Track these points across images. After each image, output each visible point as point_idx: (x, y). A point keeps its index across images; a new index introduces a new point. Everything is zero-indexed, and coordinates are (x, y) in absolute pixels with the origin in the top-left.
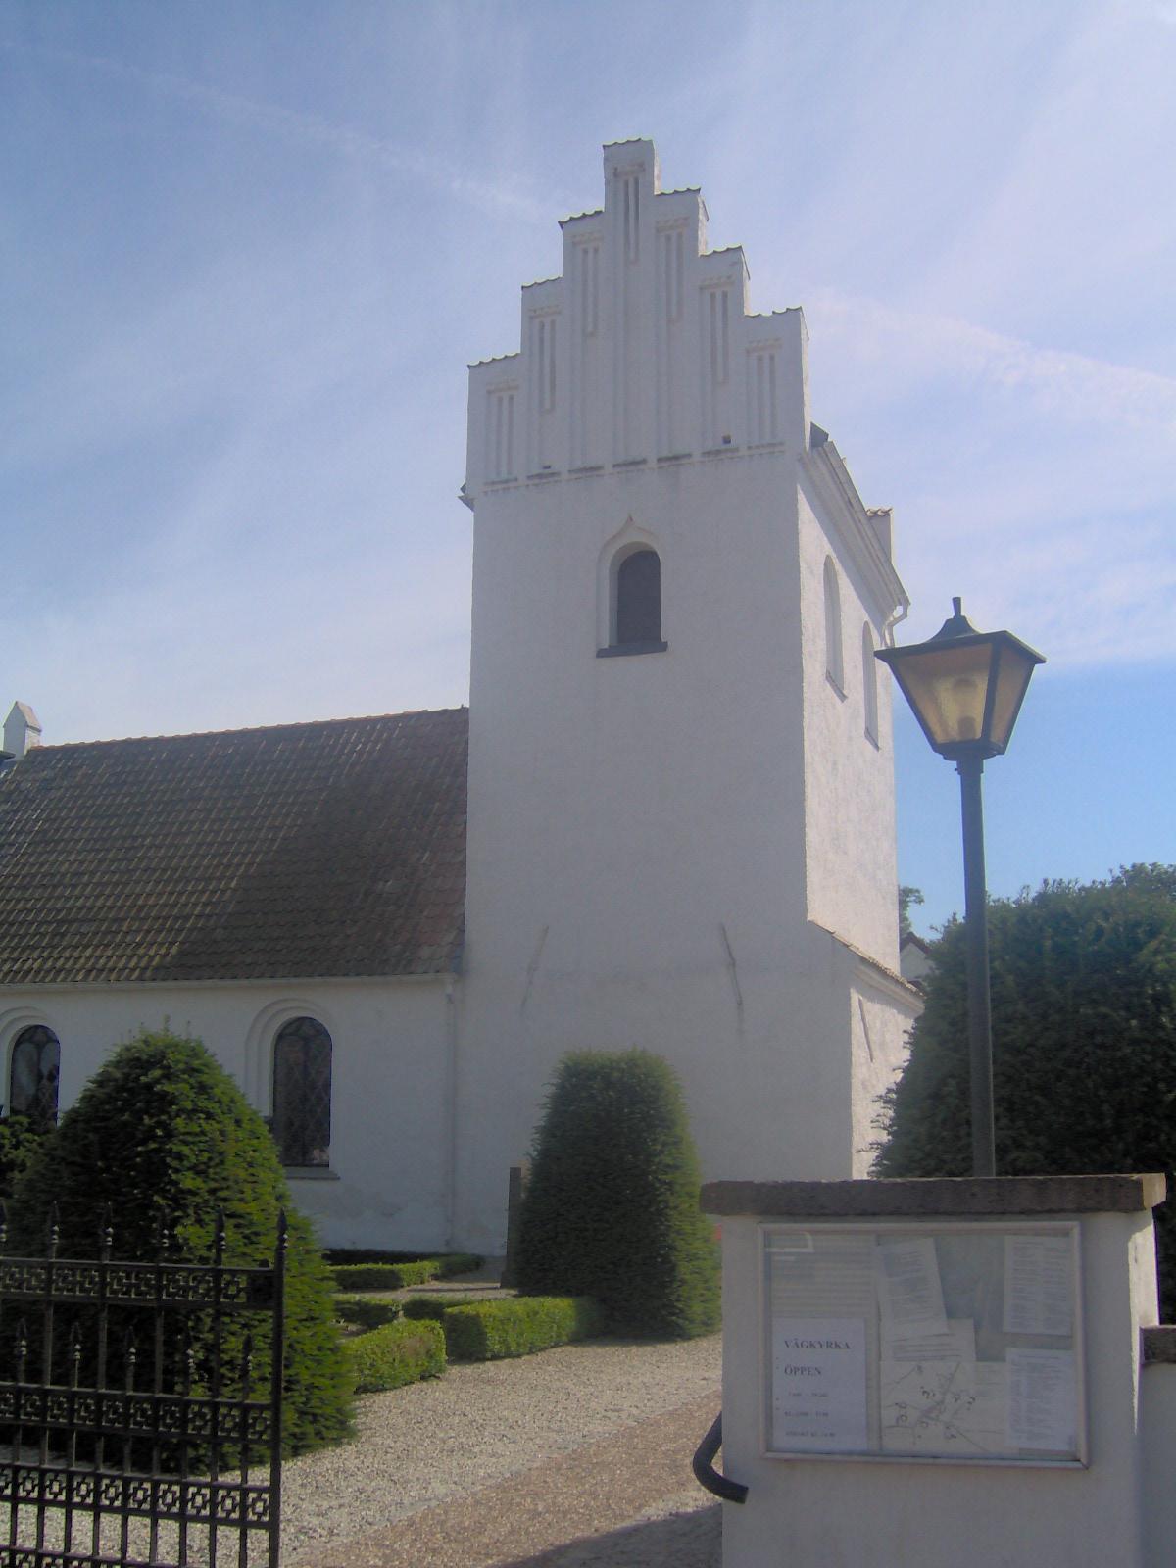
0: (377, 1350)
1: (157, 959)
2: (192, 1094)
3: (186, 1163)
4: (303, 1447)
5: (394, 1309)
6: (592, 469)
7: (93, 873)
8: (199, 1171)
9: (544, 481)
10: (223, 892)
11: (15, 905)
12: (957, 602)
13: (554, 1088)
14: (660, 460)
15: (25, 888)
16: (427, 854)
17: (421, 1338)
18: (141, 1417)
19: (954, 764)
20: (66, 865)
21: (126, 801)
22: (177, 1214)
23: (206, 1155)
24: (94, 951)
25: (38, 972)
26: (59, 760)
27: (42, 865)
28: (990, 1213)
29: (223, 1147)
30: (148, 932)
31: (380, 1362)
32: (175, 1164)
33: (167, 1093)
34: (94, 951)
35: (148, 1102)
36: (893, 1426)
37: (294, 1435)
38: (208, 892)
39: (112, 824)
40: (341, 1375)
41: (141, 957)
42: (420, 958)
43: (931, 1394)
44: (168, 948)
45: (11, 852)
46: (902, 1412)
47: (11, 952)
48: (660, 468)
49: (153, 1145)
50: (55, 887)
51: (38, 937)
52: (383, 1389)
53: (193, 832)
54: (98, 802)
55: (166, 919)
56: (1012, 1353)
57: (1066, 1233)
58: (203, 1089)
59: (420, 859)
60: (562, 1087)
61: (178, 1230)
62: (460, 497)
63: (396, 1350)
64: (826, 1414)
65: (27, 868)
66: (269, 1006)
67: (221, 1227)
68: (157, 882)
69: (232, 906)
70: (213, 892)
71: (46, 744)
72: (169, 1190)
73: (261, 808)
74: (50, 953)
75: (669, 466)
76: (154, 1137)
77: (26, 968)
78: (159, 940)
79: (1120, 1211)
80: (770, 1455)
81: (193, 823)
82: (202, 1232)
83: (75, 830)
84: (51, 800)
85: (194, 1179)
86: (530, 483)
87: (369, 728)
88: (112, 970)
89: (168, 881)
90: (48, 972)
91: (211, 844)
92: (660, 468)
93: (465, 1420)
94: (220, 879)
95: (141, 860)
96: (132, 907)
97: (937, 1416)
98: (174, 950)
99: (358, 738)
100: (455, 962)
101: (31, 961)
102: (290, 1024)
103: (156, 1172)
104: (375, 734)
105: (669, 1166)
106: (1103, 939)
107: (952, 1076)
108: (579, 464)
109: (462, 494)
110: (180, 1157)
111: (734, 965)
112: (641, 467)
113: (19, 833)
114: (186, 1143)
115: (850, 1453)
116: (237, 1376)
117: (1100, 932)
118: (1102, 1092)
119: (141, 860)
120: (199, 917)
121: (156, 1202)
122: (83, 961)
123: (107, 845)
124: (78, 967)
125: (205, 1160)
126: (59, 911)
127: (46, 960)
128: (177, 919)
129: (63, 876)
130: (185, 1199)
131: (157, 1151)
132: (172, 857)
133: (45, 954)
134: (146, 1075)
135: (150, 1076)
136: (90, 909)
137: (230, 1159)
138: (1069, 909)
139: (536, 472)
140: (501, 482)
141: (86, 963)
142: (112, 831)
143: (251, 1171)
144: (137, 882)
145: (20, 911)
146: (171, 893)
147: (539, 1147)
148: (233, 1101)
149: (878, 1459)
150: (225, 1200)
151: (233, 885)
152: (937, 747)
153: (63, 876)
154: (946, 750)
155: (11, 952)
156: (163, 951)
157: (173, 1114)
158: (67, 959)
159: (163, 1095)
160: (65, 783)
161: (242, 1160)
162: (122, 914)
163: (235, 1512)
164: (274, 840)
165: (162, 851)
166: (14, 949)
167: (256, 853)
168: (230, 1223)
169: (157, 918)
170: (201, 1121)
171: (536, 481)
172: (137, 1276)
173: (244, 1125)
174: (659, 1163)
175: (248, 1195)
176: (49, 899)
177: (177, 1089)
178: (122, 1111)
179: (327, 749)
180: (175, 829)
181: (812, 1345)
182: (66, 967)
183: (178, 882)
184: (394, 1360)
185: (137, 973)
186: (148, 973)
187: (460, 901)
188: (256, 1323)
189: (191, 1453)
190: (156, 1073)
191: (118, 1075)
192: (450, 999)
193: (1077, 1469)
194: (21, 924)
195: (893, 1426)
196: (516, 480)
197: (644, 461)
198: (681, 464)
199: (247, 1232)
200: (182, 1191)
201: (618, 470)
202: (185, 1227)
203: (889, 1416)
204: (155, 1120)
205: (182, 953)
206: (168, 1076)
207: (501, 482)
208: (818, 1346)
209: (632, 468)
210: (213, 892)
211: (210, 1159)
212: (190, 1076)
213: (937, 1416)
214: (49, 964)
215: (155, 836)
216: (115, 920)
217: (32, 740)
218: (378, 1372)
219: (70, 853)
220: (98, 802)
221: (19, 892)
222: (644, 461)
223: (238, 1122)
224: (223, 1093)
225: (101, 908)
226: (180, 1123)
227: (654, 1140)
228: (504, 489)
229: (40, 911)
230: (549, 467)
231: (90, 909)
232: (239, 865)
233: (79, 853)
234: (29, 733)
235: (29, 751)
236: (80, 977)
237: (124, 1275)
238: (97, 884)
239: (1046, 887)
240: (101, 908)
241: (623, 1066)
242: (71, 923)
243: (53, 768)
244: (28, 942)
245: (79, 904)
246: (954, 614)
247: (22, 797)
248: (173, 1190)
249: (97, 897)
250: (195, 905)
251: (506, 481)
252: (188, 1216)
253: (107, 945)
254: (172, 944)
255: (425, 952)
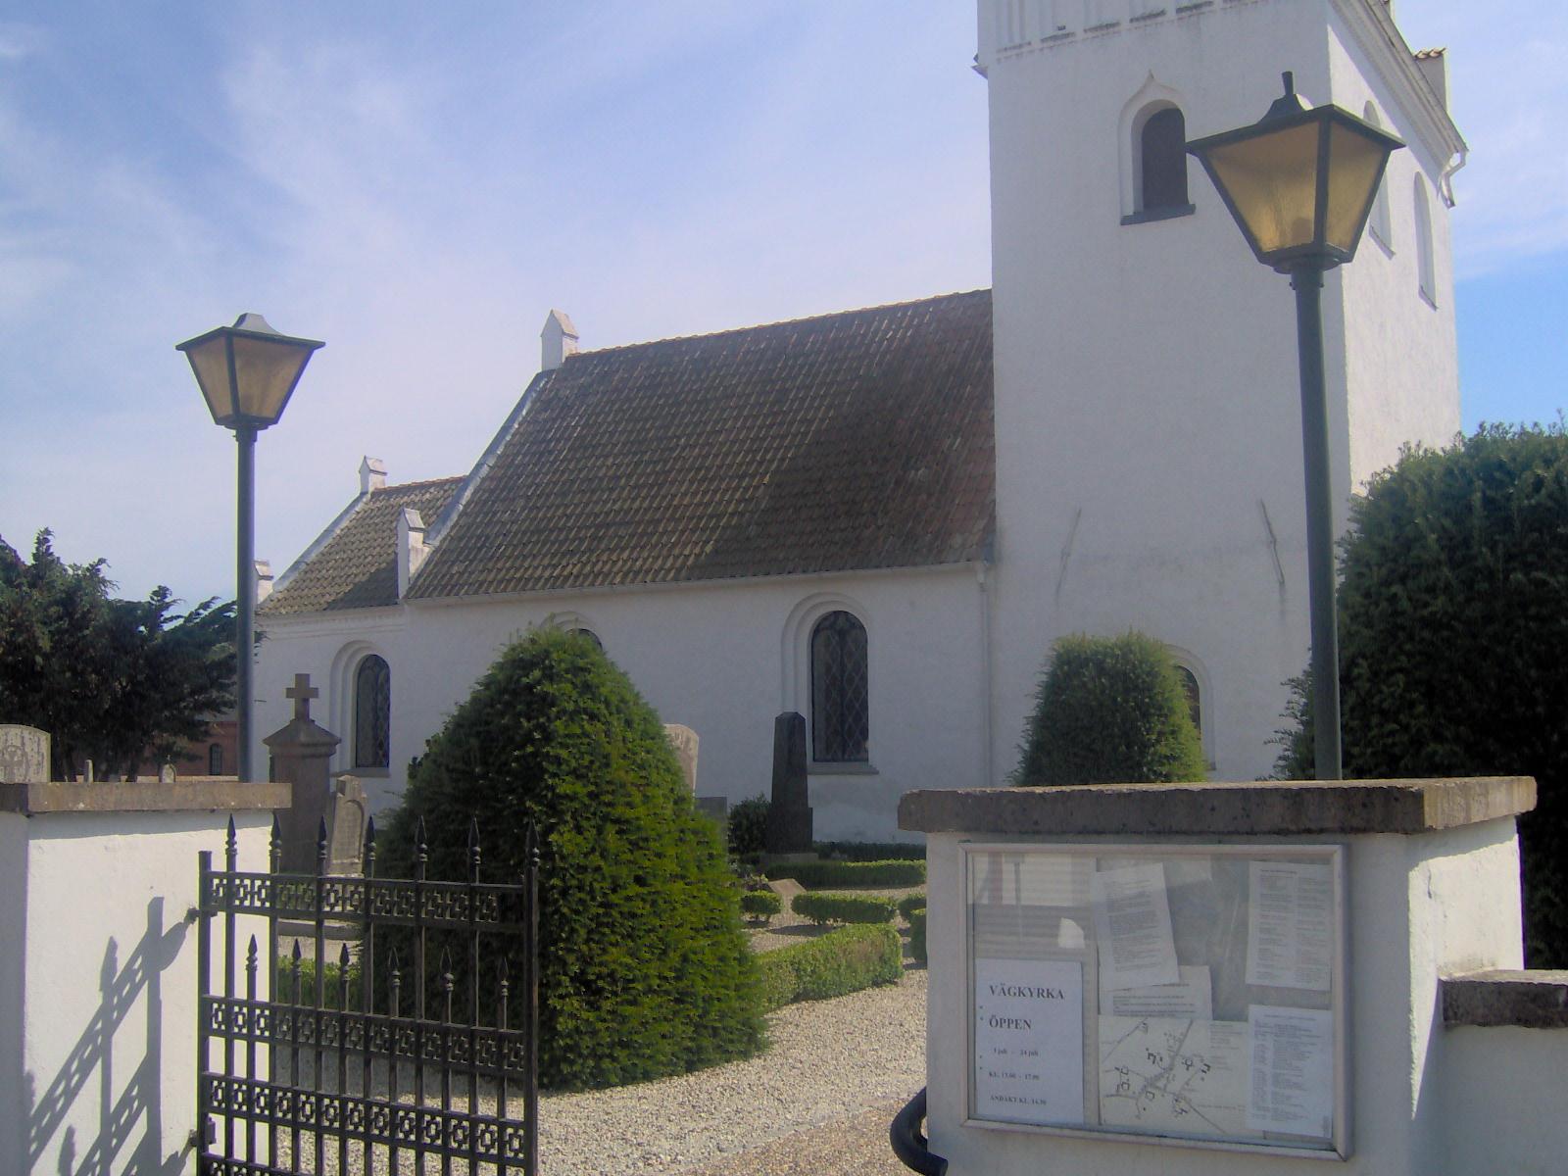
0: (819, 956)
1: (692, 559)
2: (575, 695)
3: (564, 767)
4: (701, 1061)
5: (890, 908)
6: (1108, 26)
7: (630, 476)
8: (577, 774)
9: (1059, 42)
10: (757, 488)
11: (555, 512)
12: (1288, 78)
13: (1045, 676)
14: (1179, 10)
15: (564, 494)
16: (959, 440)
17: (873, 942)
18: (406, 1044)
19: (1287, 278)
20: (604, 470)
21: (661, 402)
22: (552, 821)
23: (587, 758)
24: (631, 552)
25: (577, 577)
26: (596, 366)
27: (580, 471)
28: (1237, 832)
29: (608, 748)
30: (683, 532)
31: (822, 968)
32: (552, 768)
33: (547, 693)
34: (631, 552)
35: (529, 704)
36: (1112, 1095)
37: (688, 1049)
38: (710, 492)
39: (648, 426)
40: (749, 986)
41: (676, 558)
42: (950, 547)
43: (1158, 1058)
44: (702, 548)
45: (551, 459)
46: (1124, 1078)
47: (552, 559)
48: (1180, 19)
49: (530, 749)
50: (593, 492)
51: (577, 542)
52: (827, 997)
53: (726, 430)
54: (634, 405)
55: (700, 518)
56: (1255, 1011)
57: (1326, 860)
58: (587, 688)
59: (951, 446)
60: (1053, 675)
61: (553, 837)
62: (974, 68)
63: (841, 955)
64: (1036, 1077)
65: (566, 475)
66: (809, 598)
67: (600, 830)
68: (692, 483)
69: (765, 502)
70: (746, 489)
71: (583, 350)
72: (546, 795)
73: (793, 401)
74: (588, 558)
75: (1190, 16)
76: (532, 741)
77: (565, 573)
78: (694, 539)
79: (1391, 831)
80: (970, 1123)
81: (726, 420)
82: (579, 839)
83: (612, 434)
84: (588, 406)
85: (573, 784)
86: (1045, 45)
87: (899, 315)
88: (647, 572)
89: (703, 480)
90: (586, 577)
91: (744, 441)
92: (1180, 19)
93: (899, 1031)
94: (753, 476)
95: (676, 460)
96: (667, 509)
97: (1165, 1086)
98: (708, 548)
99: (888, 328)
100: (987, 549)
101: (571, 566)
102: (825, 618)
103: (531, 778)
104: (907, 319)
105: (1166, 757)
106: (1543, 491)
107: (1364, 656)
108: (1094, 23)
109: (976, 64)
110: (558, 761)
111: (1275, 542)
112: (1160, 19)
113: (558, 441)
114: (562, 745)
115: (1061, 1126)
116: (619, 989)
117: (1539, 483)
118: (1533, 673)
119: (676, 460)
120: (732, 515)
121: (530, 808)
122: (620, 563)
123: (643, 448)
124: (615, 569)
125: (586, 763)
126: (597, 516)
127: (585, 565)
128: (711, 517)
129: (601, 480)
130: (562, 804)
131: (534, 755)
132: (706, 457)
133: (584, 559)
134: (527, 676)
135: (531, 677)
136: (627, 512)
137: (616, 762)
138: (1504, 457)
139: (1050, 32)
140: (1014, 48)
141: (623, 566)
142: (648, 434)
143: (643, 773)
144: (672, 483)
145: (560, 518)
146: (705, 493)
147: (1030, 738)
148: (623, 701)
149: (1095, 1135)
150: (610, 804)
151: (766, 480)
152: (1263, 257)
153: (601, 480)
154: (1277, 260)
155: (552, 559)
156: (697, 550)
157: (552, 716)
158: (605, 563)
159: (544, 697)
160: (602, 388)
161: (629, 762)
162: (658, 516)
163: (493, 1147)
164: (806, 434)
165: (697, 450)
166: (554, 555)
167: (788, 449)
168: (611, 830)
169: (691, 519)
170: (585, 723)
171: (1051, 43)
172: (399, 892)
173: (635, 726)
174: (1155, 754)
175: (637, 798)
176: (587, 504)
177: (559, 690)
178: (502, 714)
179: (859, 338)
180: (709, 428)
181: (1021, 992)
182: (604, 570)
183: (712, 480)
184: (839, 966)
185: (672, 574)
186: (684, 573)
187: (991, 488)
188: (641, 934)
189: (565, 1069)
190: (537, 673)
191: (500, 677)
192: (982, 588)
193: (1334, 1160)
194: (561, 530)
195: (1112, 1095)
196: (1029, 44)
197: (1163, 13)
198: (1203, 13)
199: (633, 838)
200: (559, 796)
201: (1135, 24)
202: (562, 834)
203: (1109, 1082)
204: (534, 722)
205: (716, 551)
206: (550, 675)
207: (1014, 48)
208: (1027, 992)
209: (1148, 22)
210: (746, 489)
211: (592, 762)
212: (575, 676)
213: (1165, 1086)
214: (588, 568)
215: (689, 436)
216: (650, 522)
217: (569, 348)
218: (820, 979)
219: (607, 457)
220: (634, 405)
221: (559, 499)
222: (1163, 13)
223: (628, 723)
224: (611, 692)
225: (637, 511)
226: (558, 725)
227: (1149, 731)
228: (1017, 55)
229: (579, 516)
230: (1064, 28)
231: (627, 512)
232: (771, 461)
233: (616, 457)
234: (566, 341)
235: (567, 358)
236: (618, 580)
237: (387, 892)
238: (633, 488)
239: (1483, 431)
240: (637, 511)
241: (1118, 652)
242: (608, 526)
243: (591, 375)
244: (568, 547)
245: (616, 507)
246: (1284, 94)
247: (561, 404)
248: (550, 795)
249: (634, 500)
250: (729, 502)
251: (1021, 46)
252: (566, 822)
253: (643, 548)
254: (707, 542)
255: (957, 540)
